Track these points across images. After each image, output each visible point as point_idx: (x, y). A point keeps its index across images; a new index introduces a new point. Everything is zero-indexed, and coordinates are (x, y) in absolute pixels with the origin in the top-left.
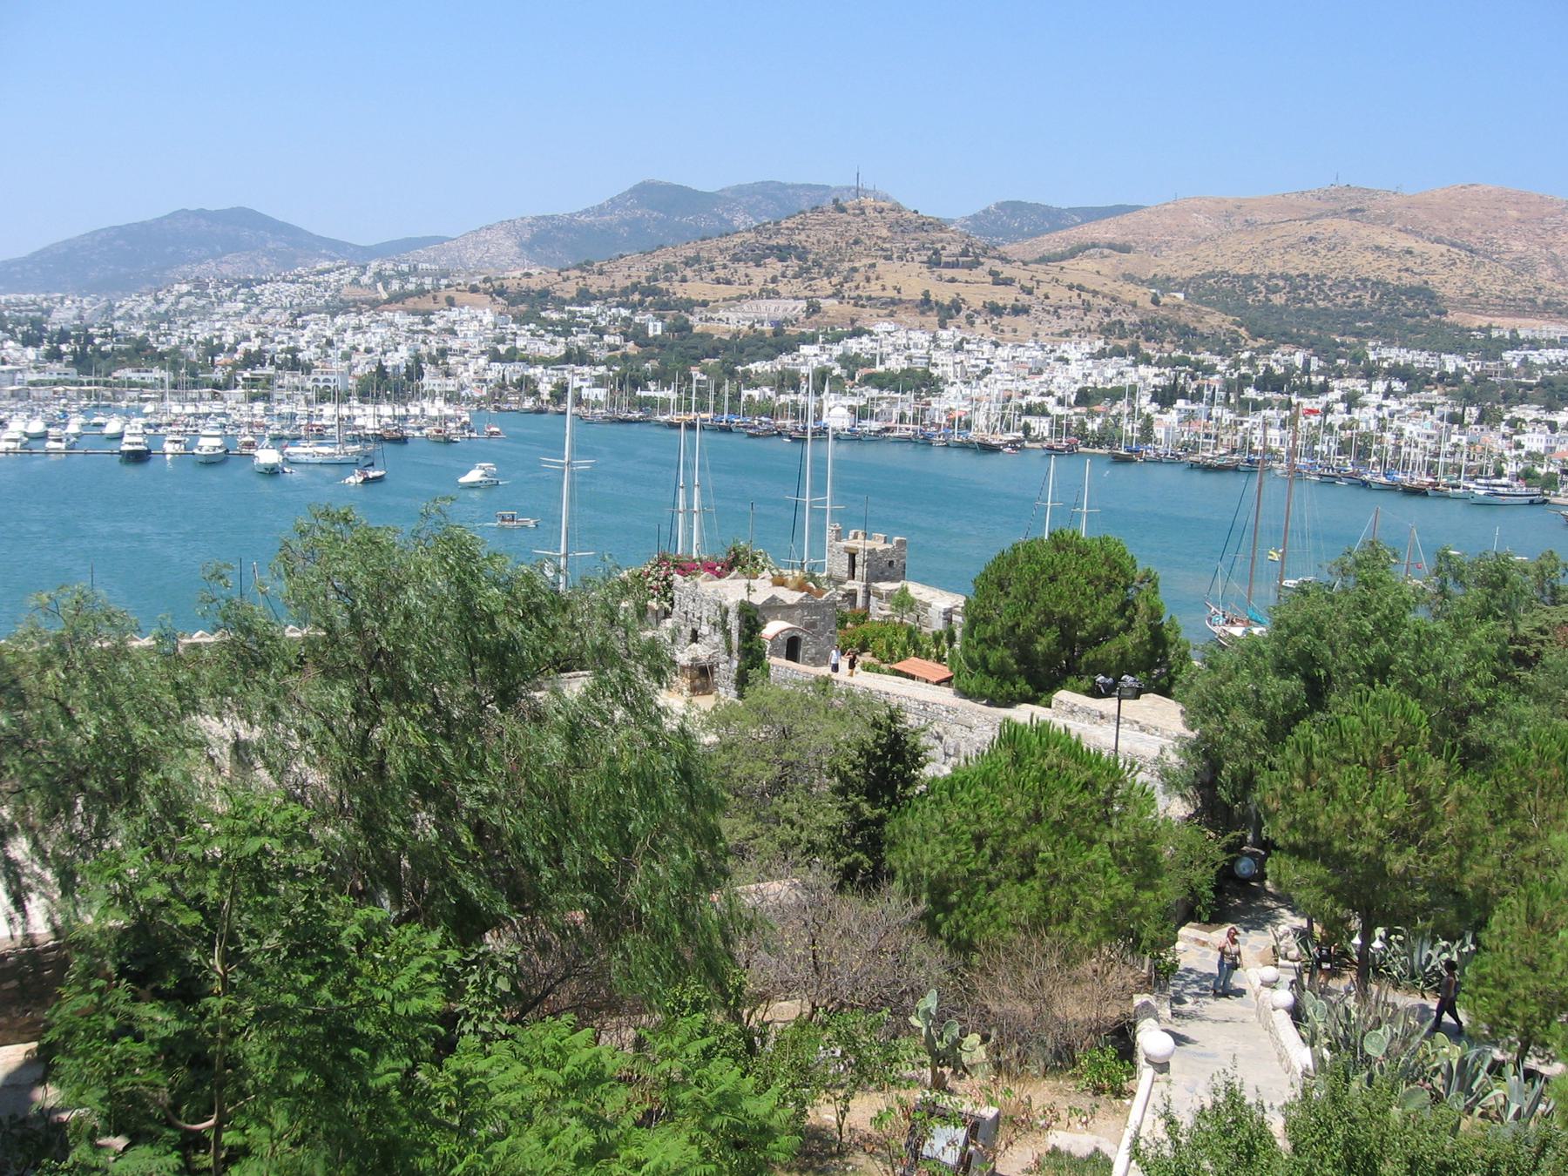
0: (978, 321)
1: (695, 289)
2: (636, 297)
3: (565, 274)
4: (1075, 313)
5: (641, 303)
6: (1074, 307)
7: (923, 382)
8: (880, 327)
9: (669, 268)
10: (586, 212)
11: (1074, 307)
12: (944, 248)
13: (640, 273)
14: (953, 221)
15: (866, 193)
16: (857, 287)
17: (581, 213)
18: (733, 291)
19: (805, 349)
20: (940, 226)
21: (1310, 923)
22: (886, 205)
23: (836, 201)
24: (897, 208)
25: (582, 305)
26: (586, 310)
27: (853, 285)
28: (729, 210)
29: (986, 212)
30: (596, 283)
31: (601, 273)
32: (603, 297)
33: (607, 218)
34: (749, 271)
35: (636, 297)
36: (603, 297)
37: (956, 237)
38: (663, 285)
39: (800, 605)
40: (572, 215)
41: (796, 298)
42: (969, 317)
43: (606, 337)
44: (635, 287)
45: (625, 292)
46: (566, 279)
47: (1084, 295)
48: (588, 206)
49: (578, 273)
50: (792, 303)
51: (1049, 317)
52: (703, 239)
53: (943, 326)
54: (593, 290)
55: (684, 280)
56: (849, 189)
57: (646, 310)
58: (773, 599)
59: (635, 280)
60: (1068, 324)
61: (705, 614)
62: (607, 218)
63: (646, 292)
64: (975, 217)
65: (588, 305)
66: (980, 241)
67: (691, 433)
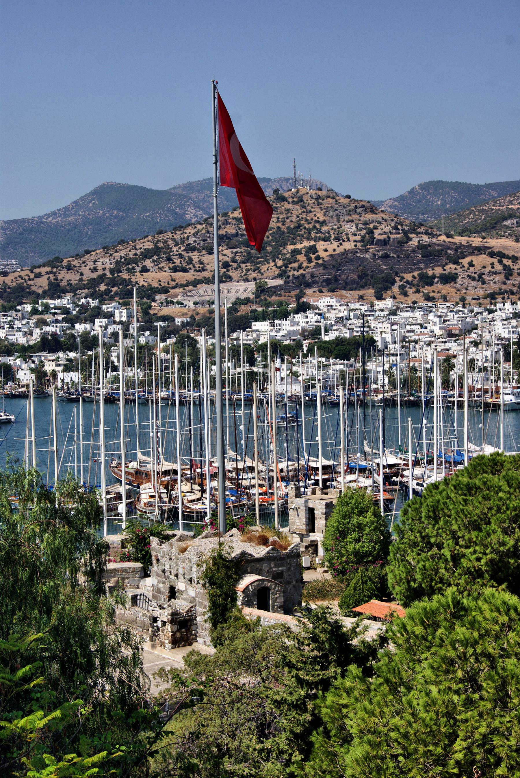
0: (410, 291)
1: (155, 276)
2: (103, 287)
3: (37, 271)
4: (497, 278)
5: (108, 292)
6: (495, 273)
7: (363, 346)
8: (324, 302)
9: (128, 261)
10: (54, 214)
11: (495, 273)
12: (376, 228)
13: (106, 263)
14: (381, 203)
15: (304, 182)
16: (300, 267)
17: (48, 216)
18: (190, 276)
19: (257, 326)
20: (372, 208)
21: (97, 705)
22: (323, 193)
23: (276, 191)
24: (332, 195)
25: (52, 298)
26: (57, 302)
27: (296, 265)
28: (181, 206)
29: (412, 192)
30: (67, 277)
31: (69, 268)
32: (73, 289)
33: (72, 218)
34: (203, 258)
35: (103, 287)
36: (73, 289)
37: (386, 217)
38: (125, 275)
39: (267, 558)
40: (40, 217)
41: (247, 280)
42: (402, 287)
43: (77, 326)
44: (102, 278)
45: (94, 283)
46: (38, 276)
47: (505, 261)
48: (54, 209)
49: (48, 269)
50: (243, 285)
51: (474, 283)
52: (160, 232)
53: (380, 297)
54: (155, 285)
55: (145, 270)
56: (287, 180)
57: (112, 299)
58: (243, 554)
59: (100, 272)
60: (494, 287)
61: (181, 571)
62: (72, 218)
63: (113, 282)
64: (401, 199)
65: (60, 297)
66: (408, 220)
67: (111, 408)
